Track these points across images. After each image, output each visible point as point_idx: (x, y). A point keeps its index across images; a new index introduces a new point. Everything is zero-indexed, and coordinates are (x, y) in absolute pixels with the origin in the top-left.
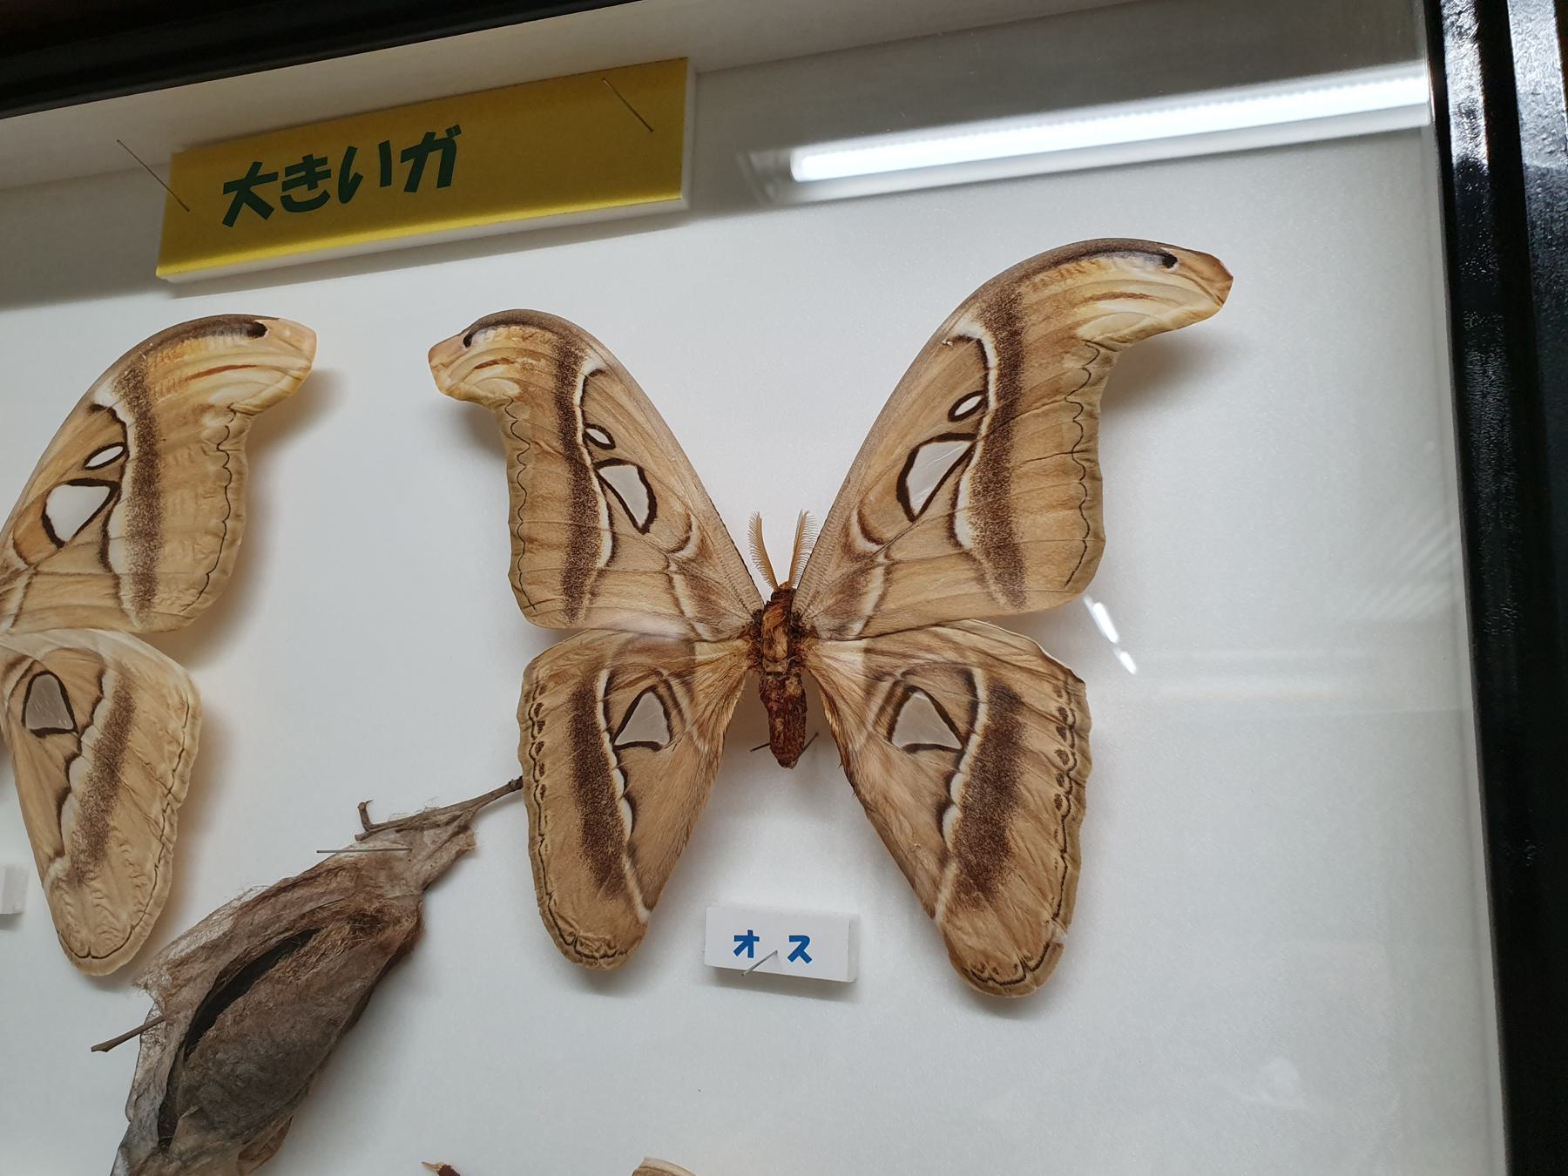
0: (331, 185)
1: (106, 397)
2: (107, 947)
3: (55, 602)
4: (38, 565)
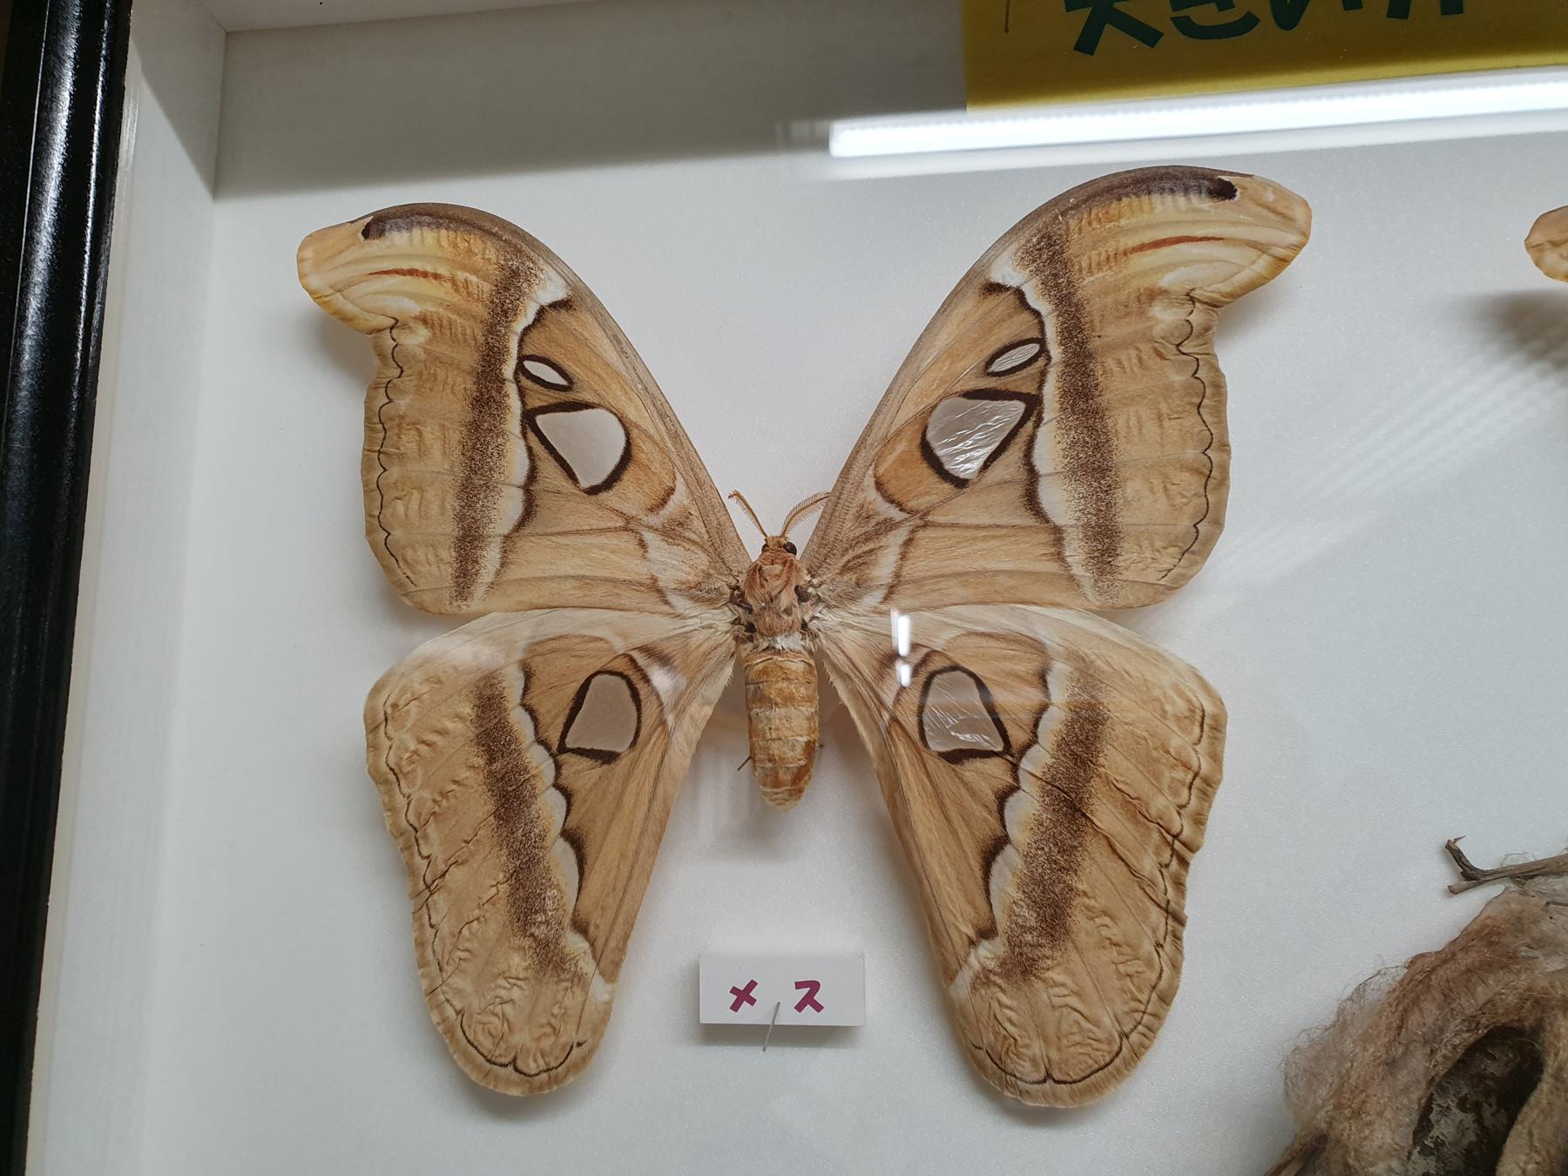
1: (1008, 272)
2: (1083, 1067)
3: (959, 566)
4: (927, 514)
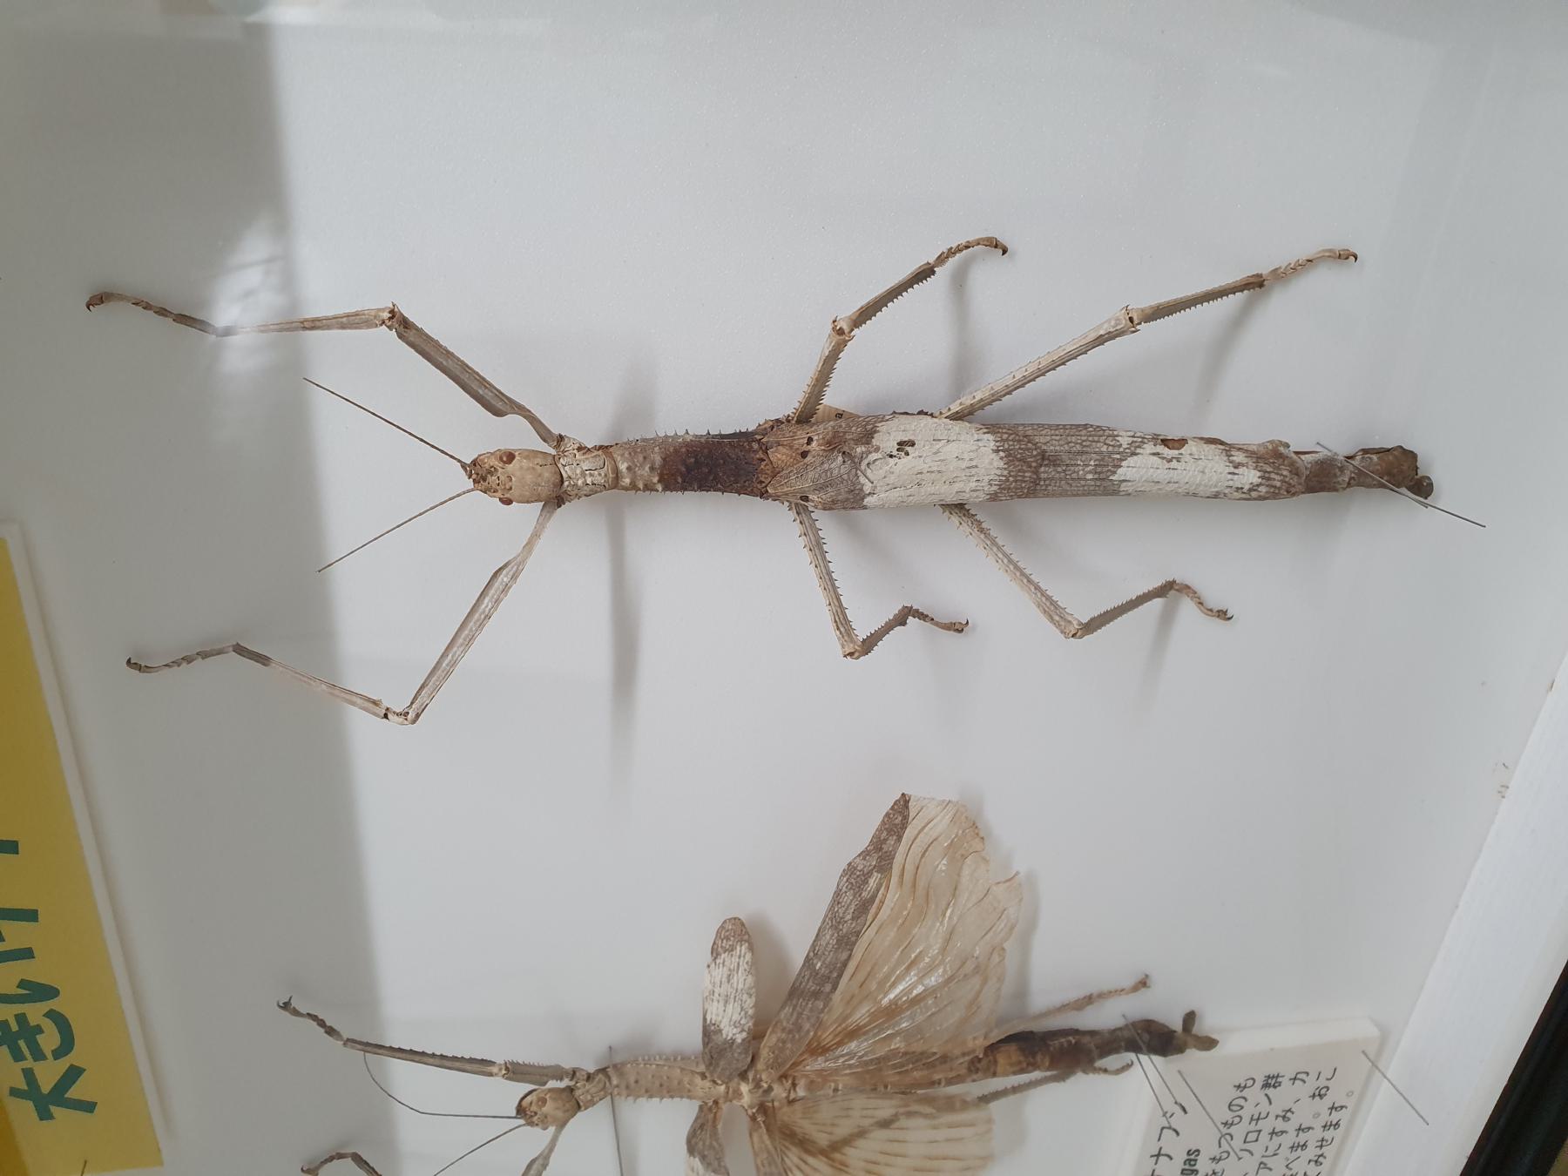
0: (35, 1013)
